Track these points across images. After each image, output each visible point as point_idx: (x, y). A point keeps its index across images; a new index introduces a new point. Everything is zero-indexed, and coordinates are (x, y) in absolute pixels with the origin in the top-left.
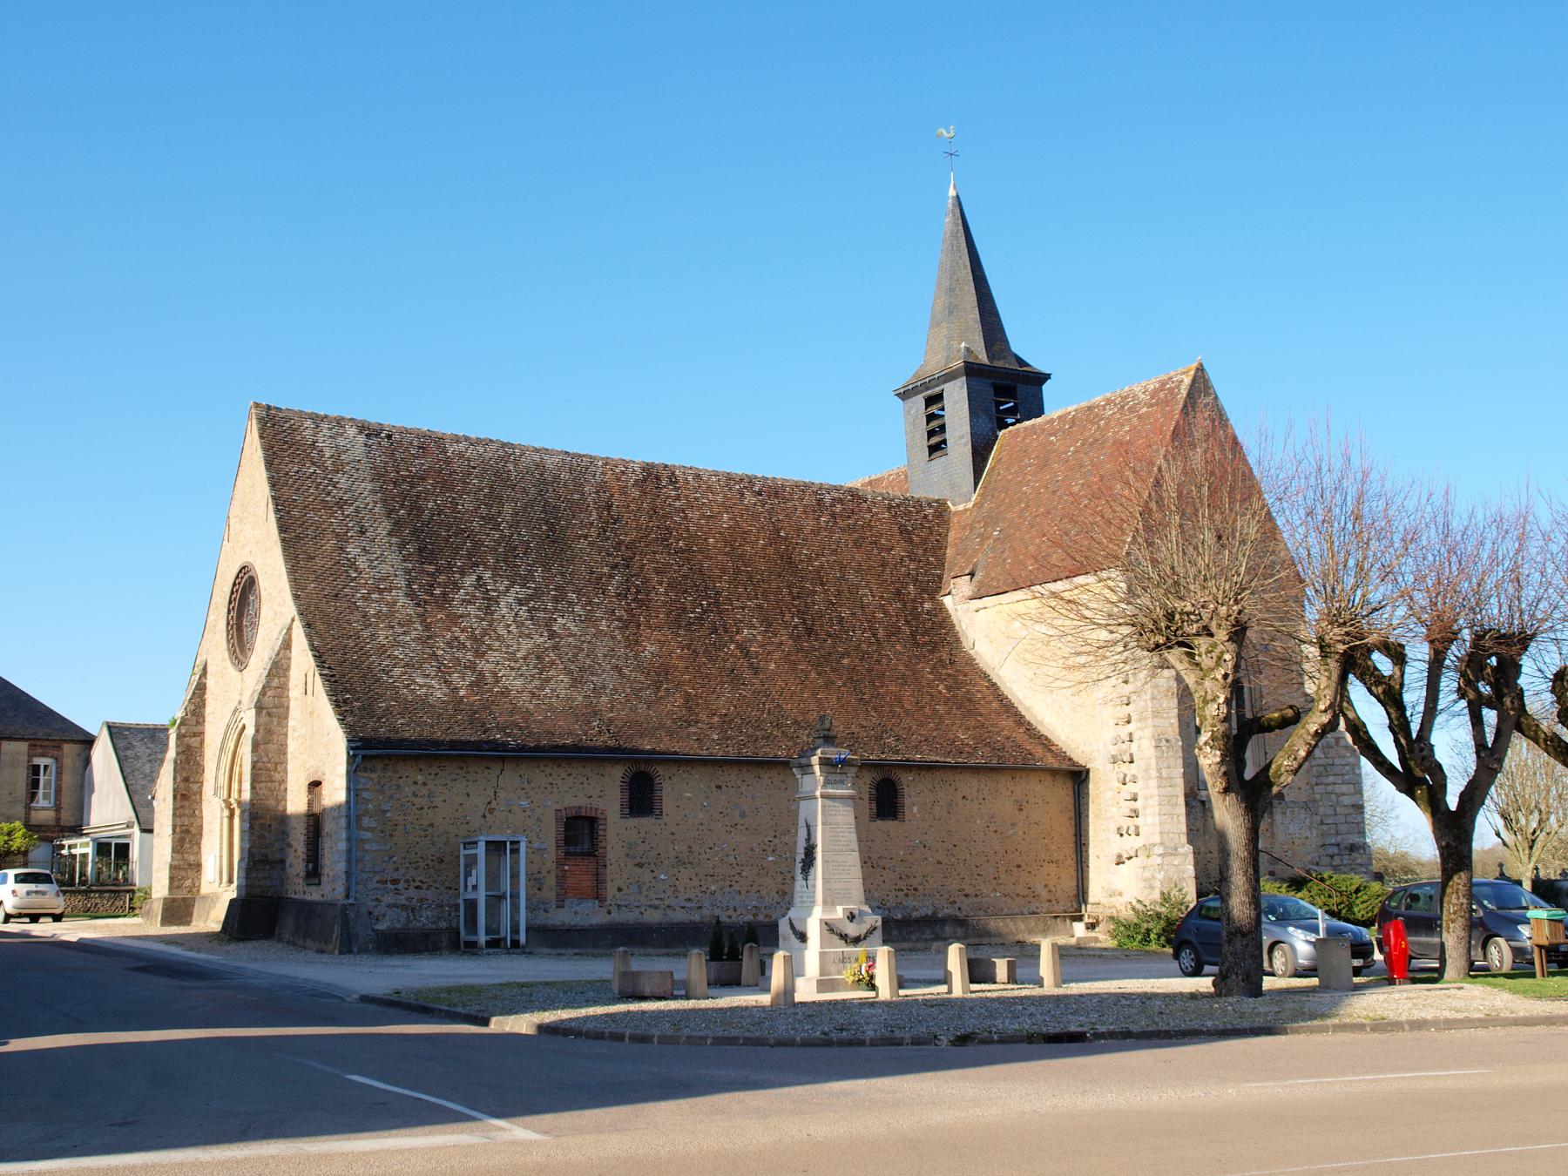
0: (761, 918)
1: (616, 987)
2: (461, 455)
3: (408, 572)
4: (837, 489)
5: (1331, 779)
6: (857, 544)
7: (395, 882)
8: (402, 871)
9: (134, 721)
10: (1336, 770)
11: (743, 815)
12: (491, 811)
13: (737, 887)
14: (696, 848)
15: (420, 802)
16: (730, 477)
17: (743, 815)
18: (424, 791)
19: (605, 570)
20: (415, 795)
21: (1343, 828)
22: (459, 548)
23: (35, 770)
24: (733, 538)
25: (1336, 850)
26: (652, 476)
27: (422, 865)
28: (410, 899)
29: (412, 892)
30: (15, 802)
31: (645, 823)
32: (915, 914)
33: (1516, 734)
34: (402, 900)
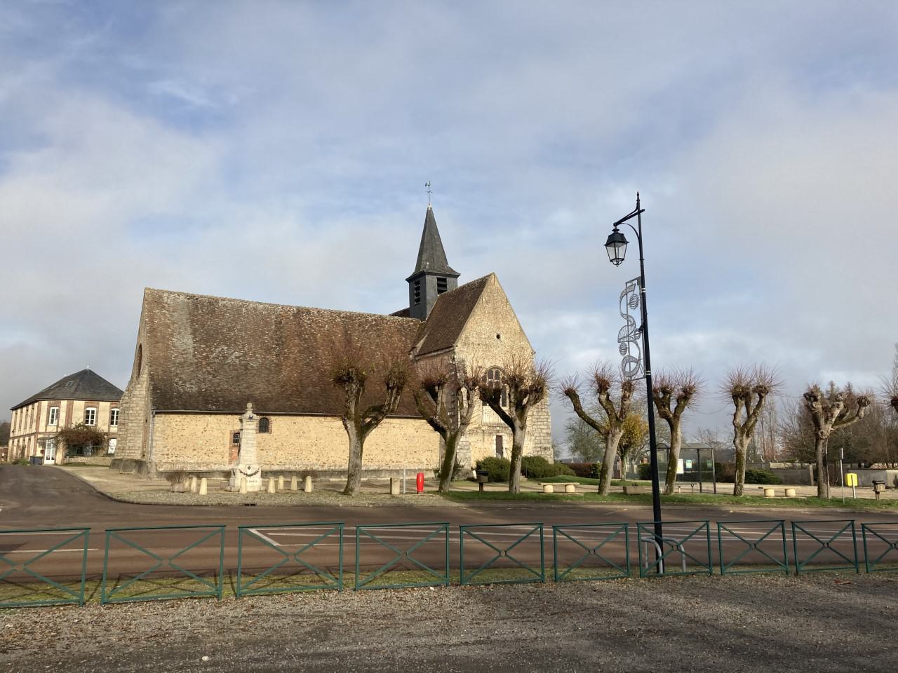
0: (308, 469)
1: (301, 480)
2: (224, 306)
3: (194, 347)
4: (374, 315)
5: (539, 423)
6: (378, 336)
7: (167, 455)
8: (171, 451)
9: (18, 404)
10: (540, 420)
11: (304, 433)
12: (205, 431)
13: (300, 458)
14: (285, 444)
15: (178, 427)
16: (332, 312)
17: (304, 433)
18: (180, 424)
19: (273, 346)
20: (176, 425)
21: (543, 441)
22: (217, 338)
23: (113, 412)
24: (329, 334)
25: (539, 449)
26: (300, 312)
27: (178, 449)
28: (173, 461)
29: (174, 458)
30: (104, 424)
31: (265, 435)
32: (371, 468)
33: (200, 493)
34: (170, 461)
